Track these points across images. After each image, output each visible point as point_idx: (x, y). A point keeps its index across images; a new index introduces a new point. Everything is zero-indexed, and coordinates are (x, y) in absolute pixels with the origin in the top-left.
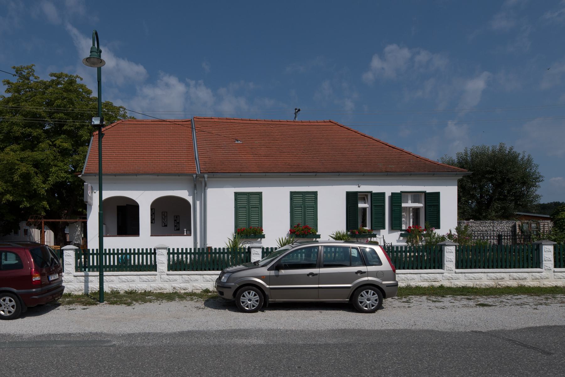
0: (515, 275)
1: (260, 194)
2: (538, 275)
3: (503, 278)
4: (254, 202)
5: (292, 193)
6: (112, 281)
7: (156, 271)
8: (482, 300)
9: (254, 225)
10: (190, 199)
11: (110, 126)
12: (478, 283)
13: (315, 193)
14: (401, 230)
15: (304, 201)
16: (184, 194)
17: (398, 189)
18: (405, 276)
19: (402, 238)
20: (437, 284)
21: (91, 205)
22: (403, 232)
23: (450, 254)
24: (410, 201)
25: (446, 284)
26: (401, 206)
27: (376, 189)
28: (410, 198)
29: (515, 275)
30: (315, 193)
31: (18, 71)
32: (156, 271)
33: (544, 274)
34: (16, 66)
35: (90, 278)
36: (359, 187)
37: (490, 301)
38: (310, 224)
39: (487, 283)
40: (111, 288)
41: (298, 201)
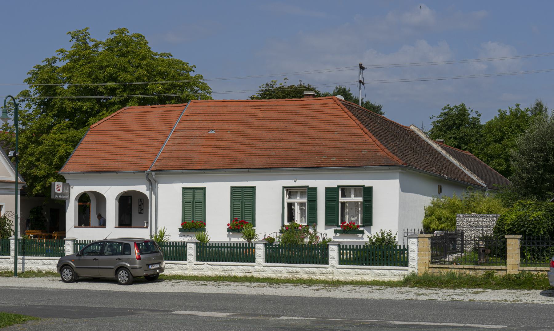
0: (307, 270)
1: (204, 189)
2: (324, 270)
3: (297, 272)
4: (199, 196)
5: (233, 188)
6: (38, 263)
7: (254, 262)
8: (202, 282)
9: (198, 219)
10: (147, 193)
11: (110, 117)
12: (279, 275)
13: (254, 188)
14: (338, 226)
15: (243, 196)
16: (143, 189)
17: (334, 183)
18: (227, 267)
19: (338, 235)
20: (249, 275)
21: (76, 199)
22: (339, 229)
23: (260, 251)
24: (353, 196)
25: (256, 275)
26: (364, 198)
27: (311, 183)
28: (353, 192)
29: (307, 270)
30: (254, 188)
31: (74, 36)
32: (254, 262)
33: (330, 270)
34: (71, 31)
35: (26, 261)
36: (295, 181)
37: (208, 283)
38: (248, 219)
39: (285, 275)
40: (38, 268)
41: (238, 196)
